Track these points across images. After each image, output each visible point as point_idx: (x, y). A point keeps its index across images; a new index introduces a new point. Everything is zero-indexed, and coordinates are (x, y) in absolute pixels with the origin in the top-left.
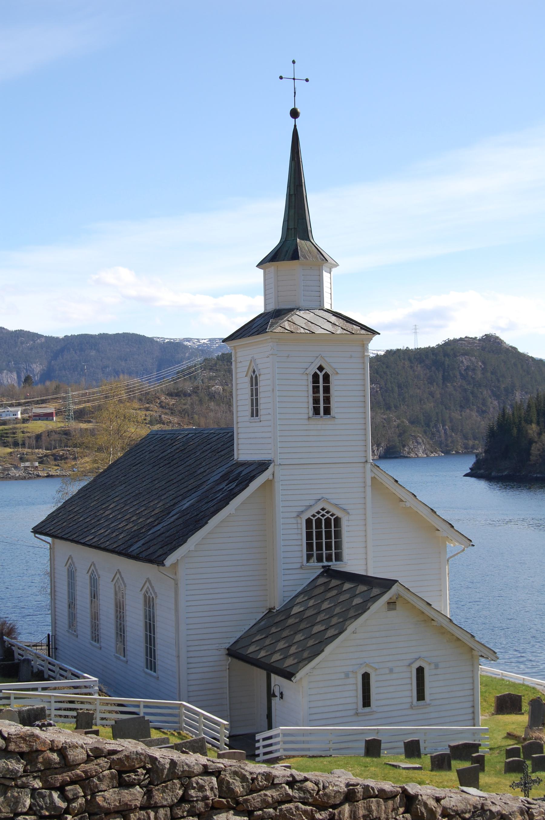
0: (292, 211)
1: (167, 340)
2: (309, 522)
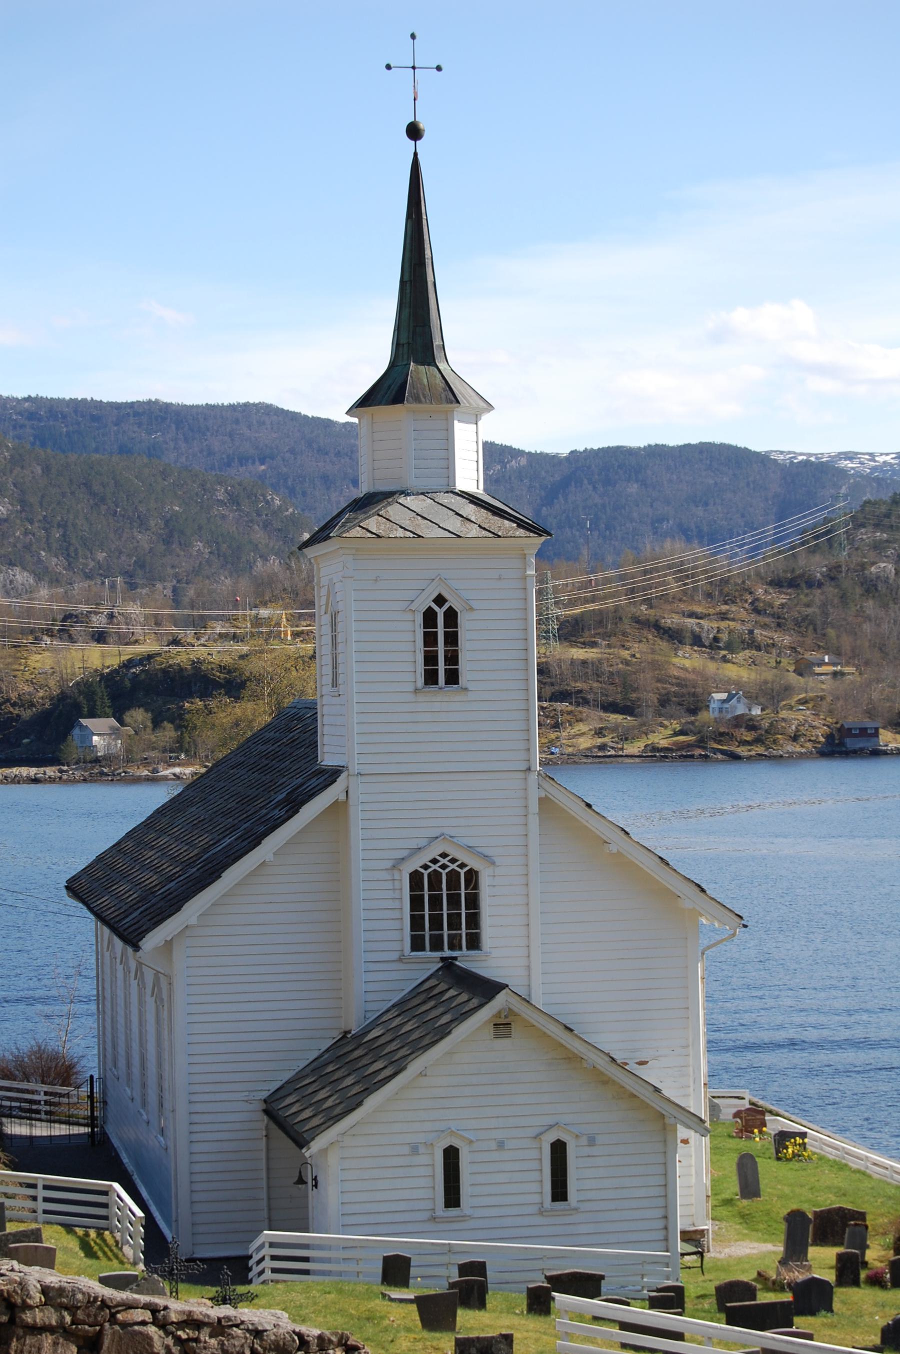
0: (406, 312)
1: (800, 458)
2: (415, 879)
